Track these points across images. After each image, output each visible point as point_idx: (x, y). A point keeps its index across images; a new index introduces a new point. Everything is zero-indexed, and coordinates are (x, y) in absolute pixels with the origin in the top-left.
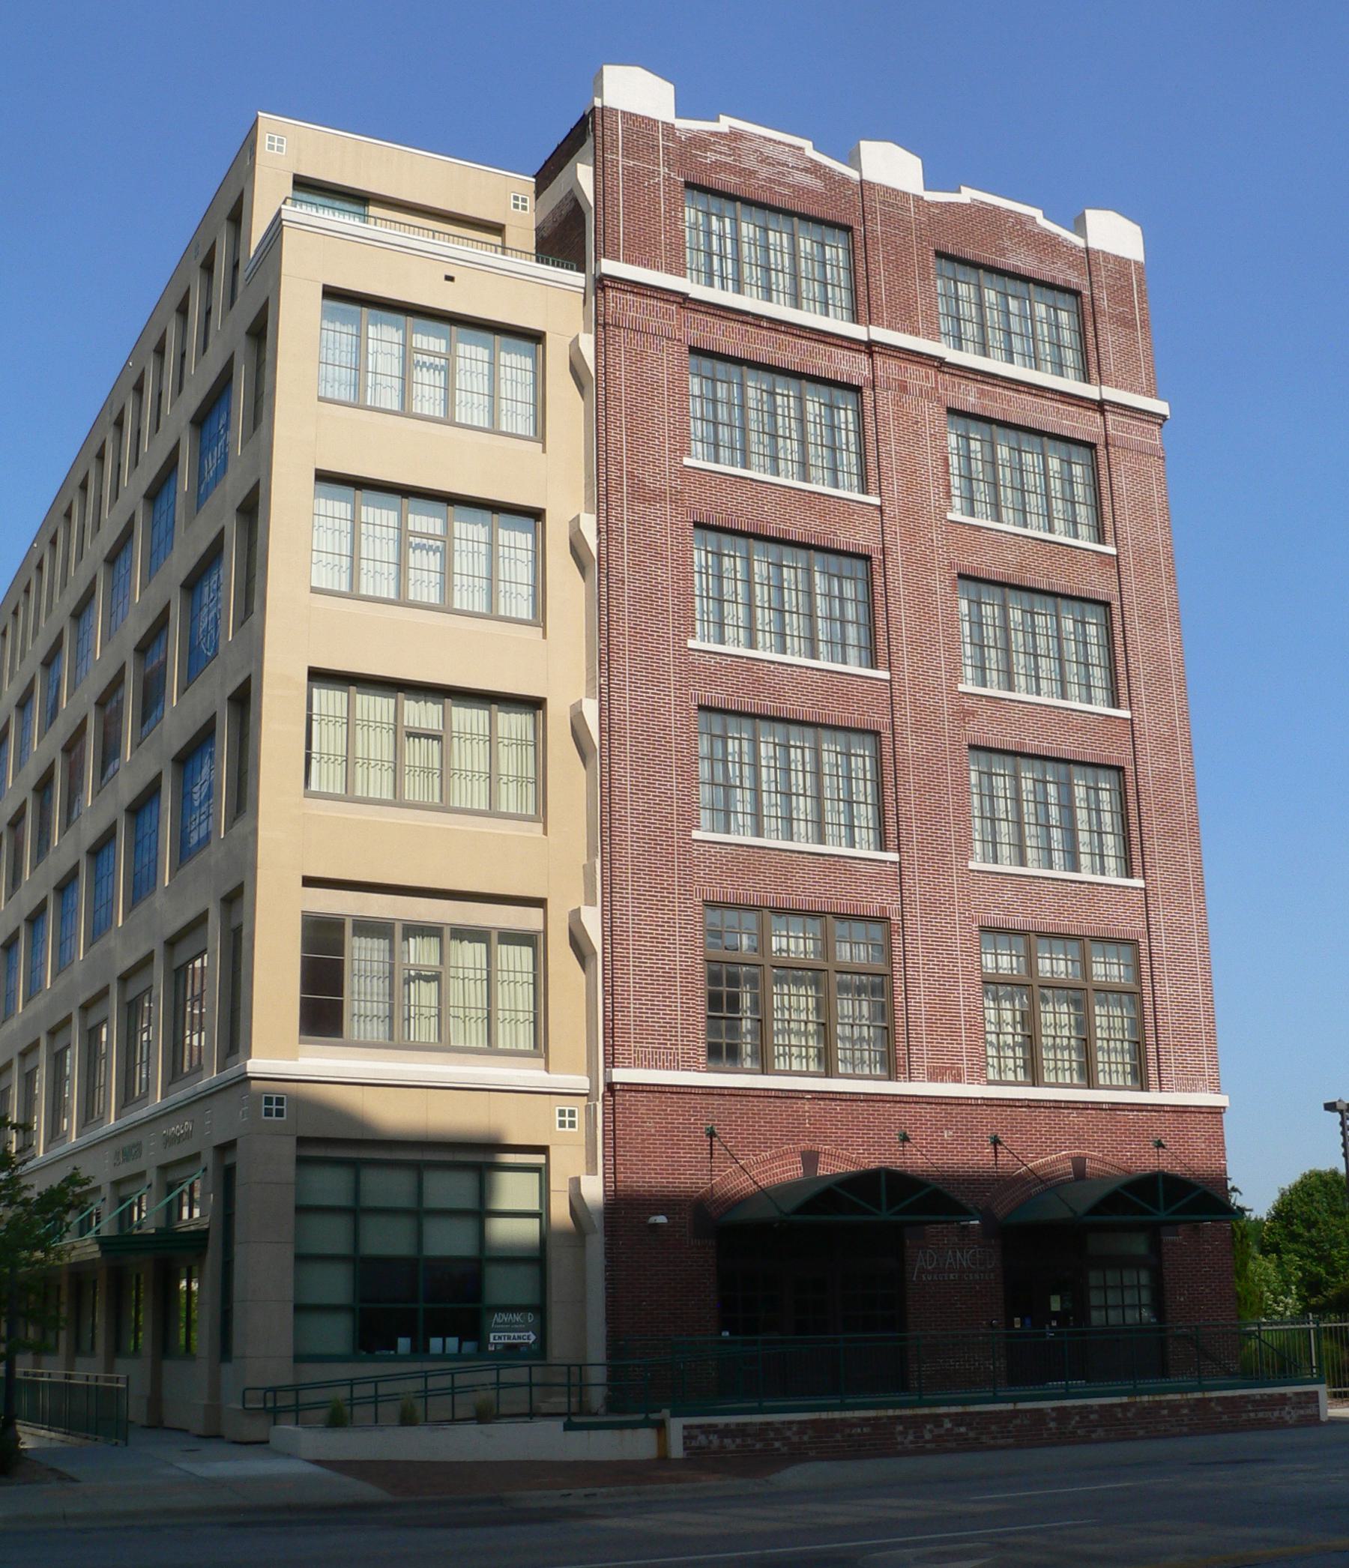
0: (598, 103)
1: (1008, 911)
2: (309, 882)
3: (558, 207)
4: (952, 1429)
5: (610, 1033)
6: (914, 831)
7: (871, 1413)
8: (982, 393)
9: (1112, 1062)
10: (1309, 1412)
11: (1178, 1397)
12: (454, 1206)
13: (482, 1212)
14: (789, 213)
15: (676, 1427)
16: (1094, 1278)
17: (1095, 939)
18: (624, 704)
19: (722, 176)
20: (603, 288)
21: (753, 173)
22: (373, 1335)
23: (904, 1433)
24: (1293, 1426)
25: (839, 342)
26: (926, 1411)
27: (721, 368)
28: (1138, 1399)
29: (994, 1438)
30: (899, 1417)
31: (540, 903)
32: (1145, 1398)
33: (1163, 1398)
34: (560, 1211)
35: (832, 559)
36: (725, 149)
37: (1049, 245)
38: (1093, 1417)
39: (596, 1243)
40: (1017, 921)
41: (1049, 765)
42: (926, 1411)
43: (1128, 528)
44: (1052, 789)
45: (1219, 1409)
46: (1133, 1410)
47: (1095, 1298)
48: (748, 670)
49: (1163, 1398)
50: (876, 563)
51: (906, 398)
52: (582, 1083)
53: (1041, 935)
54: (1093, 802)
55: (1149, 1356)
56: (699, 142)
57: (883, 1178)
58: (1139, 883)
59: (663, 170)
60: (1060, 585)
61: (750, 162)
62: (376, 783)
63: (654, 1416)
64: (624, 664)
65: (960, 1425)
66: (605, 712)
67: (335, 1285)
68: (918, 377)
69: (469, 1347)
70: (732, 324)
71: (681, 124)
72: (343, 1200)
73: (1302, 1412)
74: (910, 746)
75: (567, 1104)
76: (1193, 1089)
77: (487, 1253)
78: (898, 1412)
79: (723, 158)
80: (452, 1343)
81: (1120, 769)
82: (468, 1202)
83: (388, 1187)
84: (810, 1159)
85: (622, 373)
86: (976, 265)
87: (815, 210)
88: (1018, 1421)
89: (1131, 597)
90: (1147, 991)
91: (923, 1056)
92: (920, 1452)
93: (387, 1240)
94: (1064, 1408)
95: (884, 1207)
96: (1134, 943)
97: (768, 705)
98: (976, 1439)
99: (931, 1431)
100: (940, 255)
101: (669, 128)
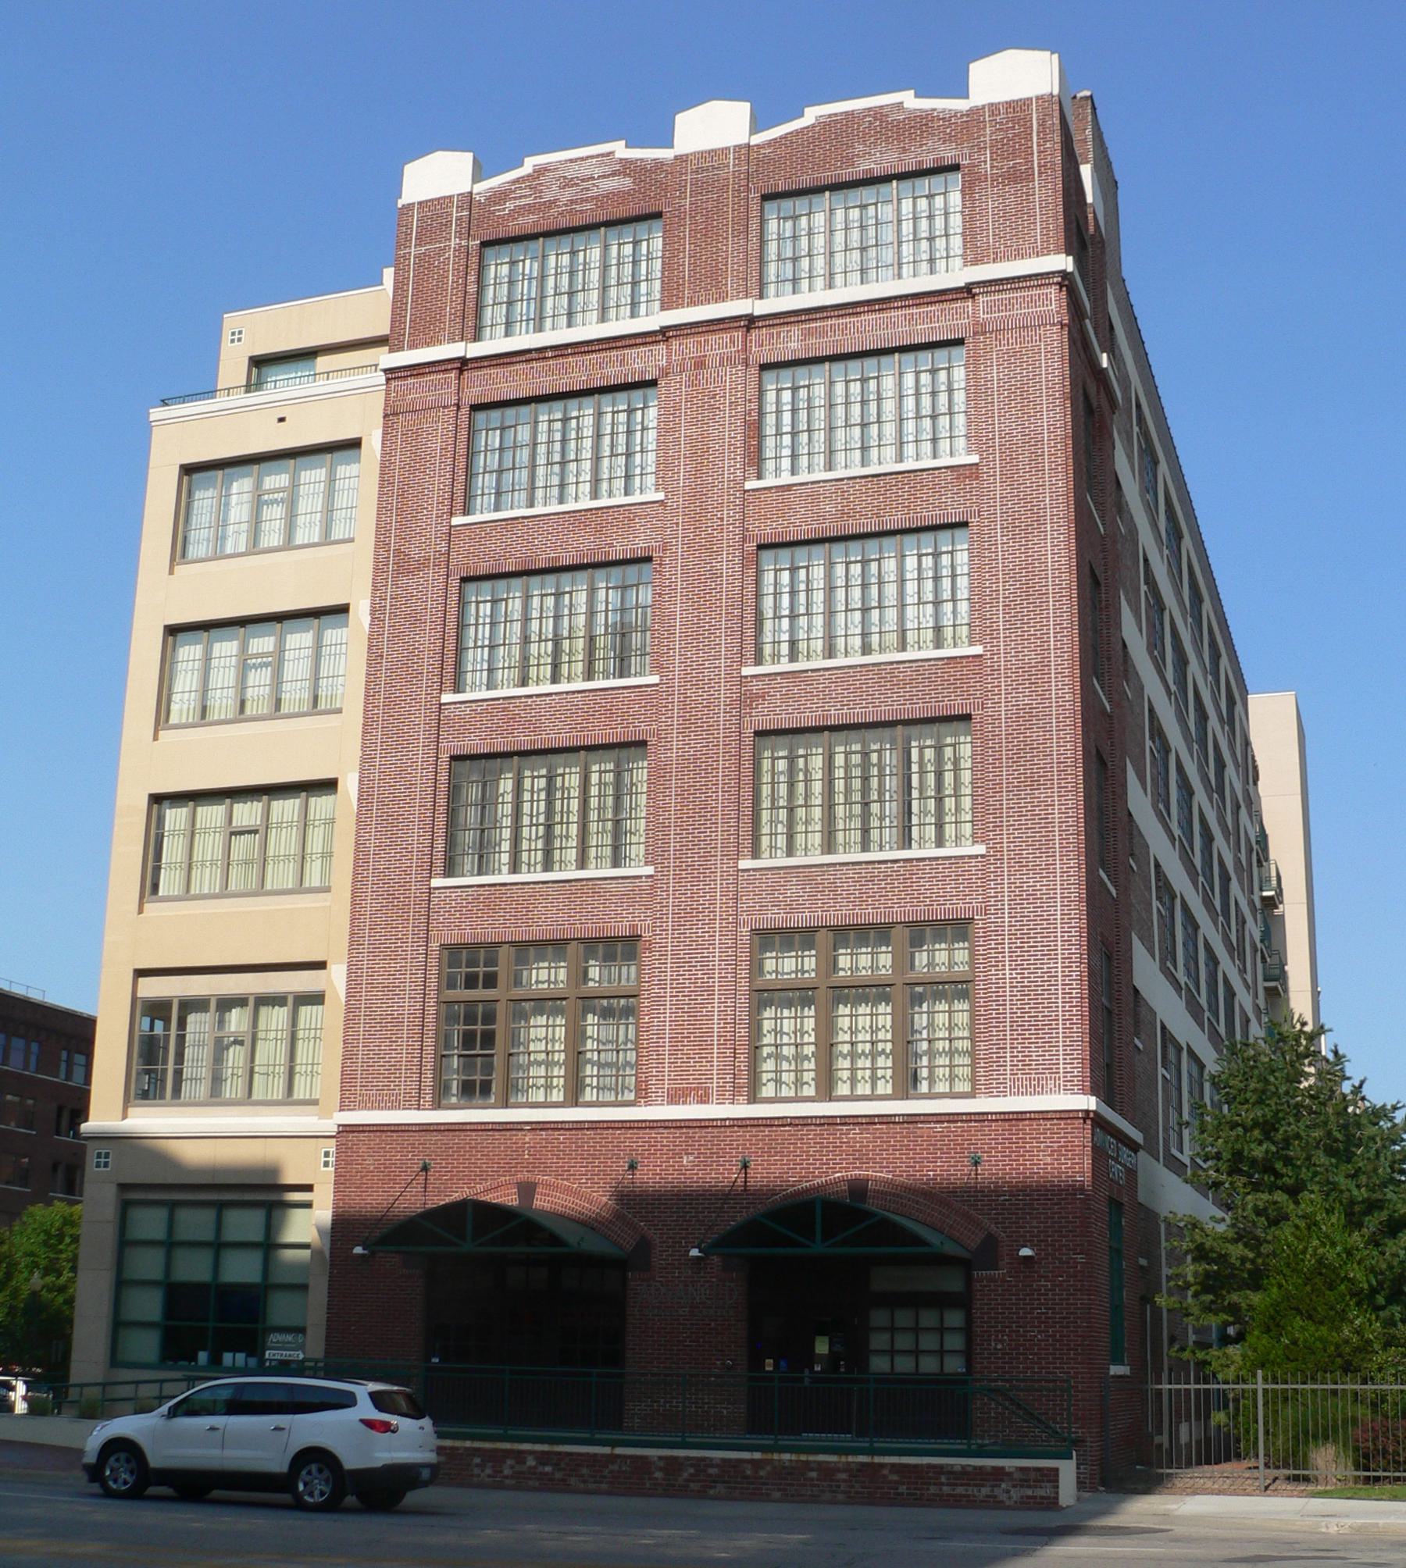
4: (535, 1467)
10: (1040, 1492)
11: (833, 1458)
19: (521, 220)
21: (552, 203)
22: (177, 1347)
23: (482, 1466)
24: (1009, 1508)
25: (633, 342)
26: (507, 1446)
28: (776, 1456)
29: (585, 1482)
30: (478, 1449)
32: (786, 1456)
33: (811, 1458)
35: (616, 572)
36: (527, 192)
38: (712, 1471)
42: (507, 1446)
45: (895, 1477)
46: (769, 1468)
47: (879, 1341)
48: (504, 709)
49: (811, 1458)
55: (935, 1410)
57: (470, 1210)
62: (206, 880)
65: (544, 1464)
67: (148, 1305)
70: (518, 367)
72: (208, 1235)
73: (1029, 1492)
76: (1038, 1089)
77: (277, 1278)
78: (477, 1444)
79: (523, 202)
80: (240, 1357)
82: (257, 1236)
83: (195, 1224)
88: (616, 1467)
92: (500, 1486)
93: (193, 1268)
94: (675, 1458)
95: (818, 1236)
97: (523, 740)
98: (564, 1480)
99: (512, 1467)
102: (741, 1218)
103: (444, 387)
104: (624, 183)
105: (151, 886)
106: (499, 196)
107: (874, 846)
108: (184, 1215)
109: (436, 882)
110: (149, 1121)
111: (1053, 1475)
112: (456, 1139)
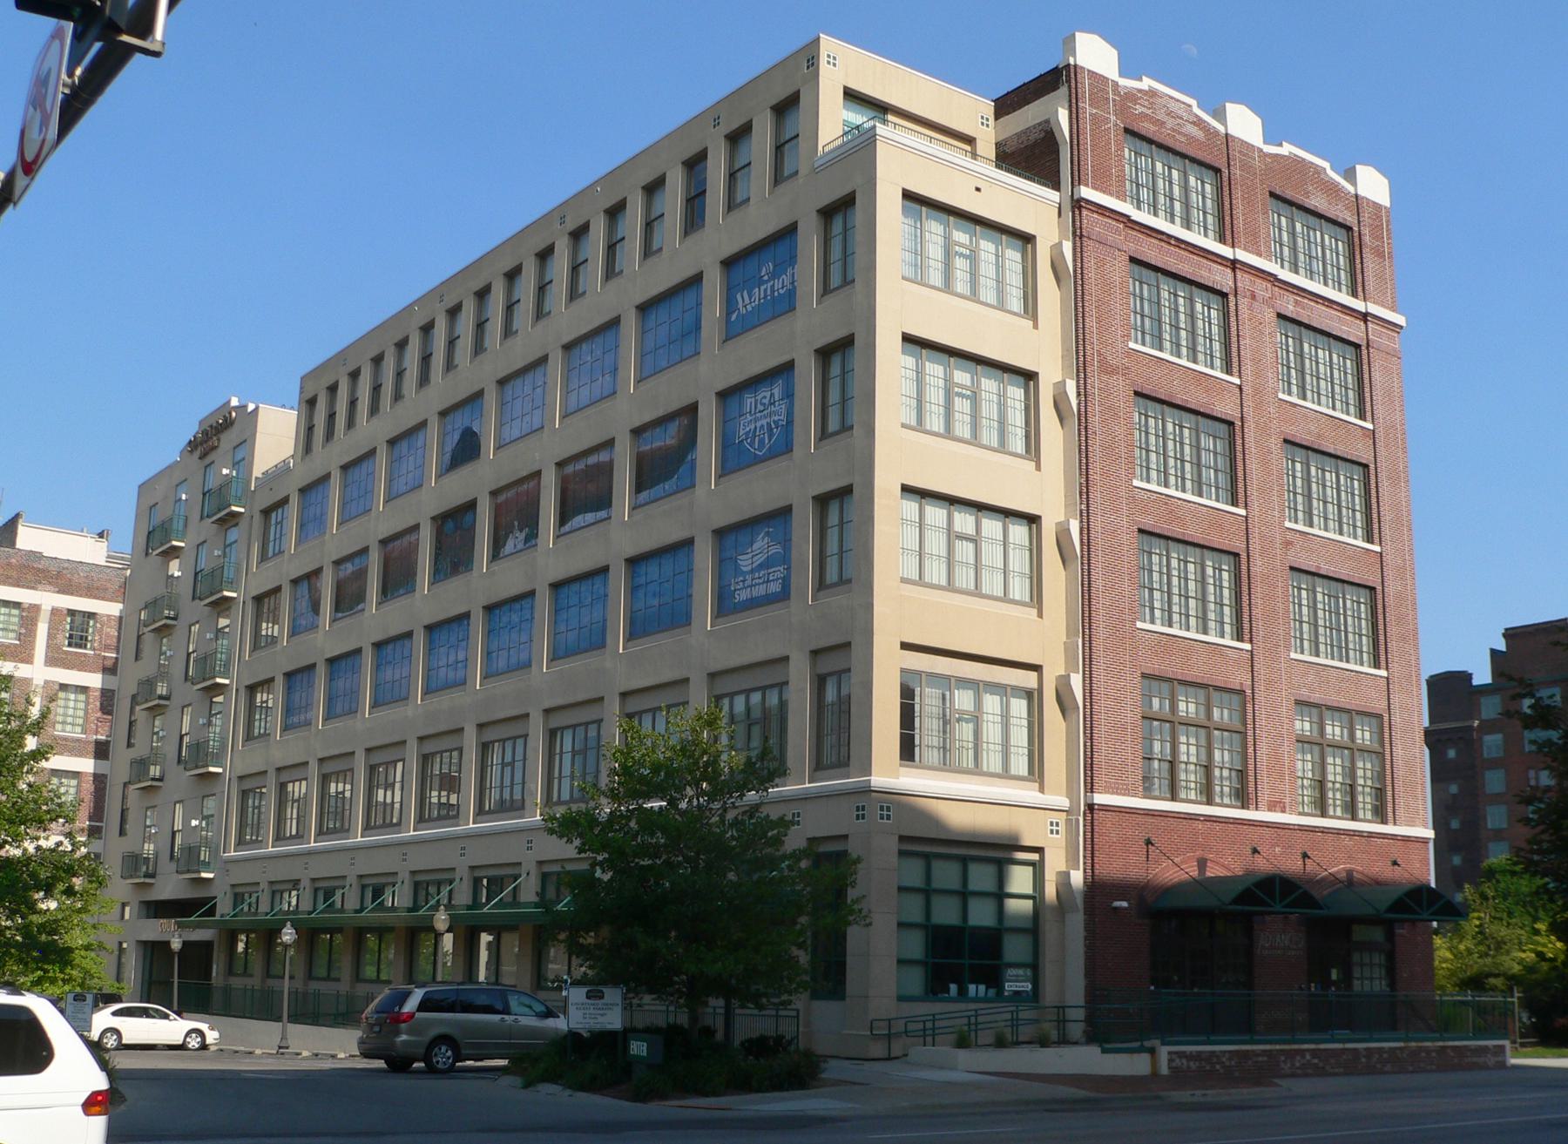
0: (1072, 61)
1: (1312, 691)
2: (905, 646)
3: (1024, 132)
5: (1090, 767)
6: (1259, 626)
7: (1268, 1047)
8: (1296, 302)
13: (1000, 895)
14: (1183, 156)
15: (1164, 1052)
16: (1356, 957)
17: (1359, 713)
18: (1097, 524)
19: (1145, 124)
20: (1080, 208)
27: (1145, 272)
31: (1036, 668)
32: (1413, 1044)
34: (1050, 891)
37: (1333, 190)
39: (1077, 922)
40: (1316, 697)
41: (1304, 577)
43: (1380, 410)
44: (1191, 567)
50: (1238, 428)
51: (1256, 304)
52: (1064, 802)
53: (1329, 708)
54: (1355, 607)
56: (1131, 96)
58: (1383, 673)
59: (1113, 118)
61: (1161, 116)
63: (1147, 1044)
64: (1096, 495)
66: (1086, 530)
68: (1261, 288)
69: (992, 992)
71: (1123, 82)
74: (1258, 566)
75: (1056, 817)
77: (1007, 924)
81: (1372, 589)
84: (1202, 864)
85: (1091, 274)
86: (1291, 203)
87: (1200, 155)
89: (1382, 464)
90: (1388, 751)
91: (1265, 795)
93: (946, 913)
96: (1380, 717)
97: (1176, 530)
100: (1272, 194)
101: (1116, 84)
102: (1241, 888)
104: (1199, 134)
107: (1176, 625)
108: (938, 867)
110: (909, 780)
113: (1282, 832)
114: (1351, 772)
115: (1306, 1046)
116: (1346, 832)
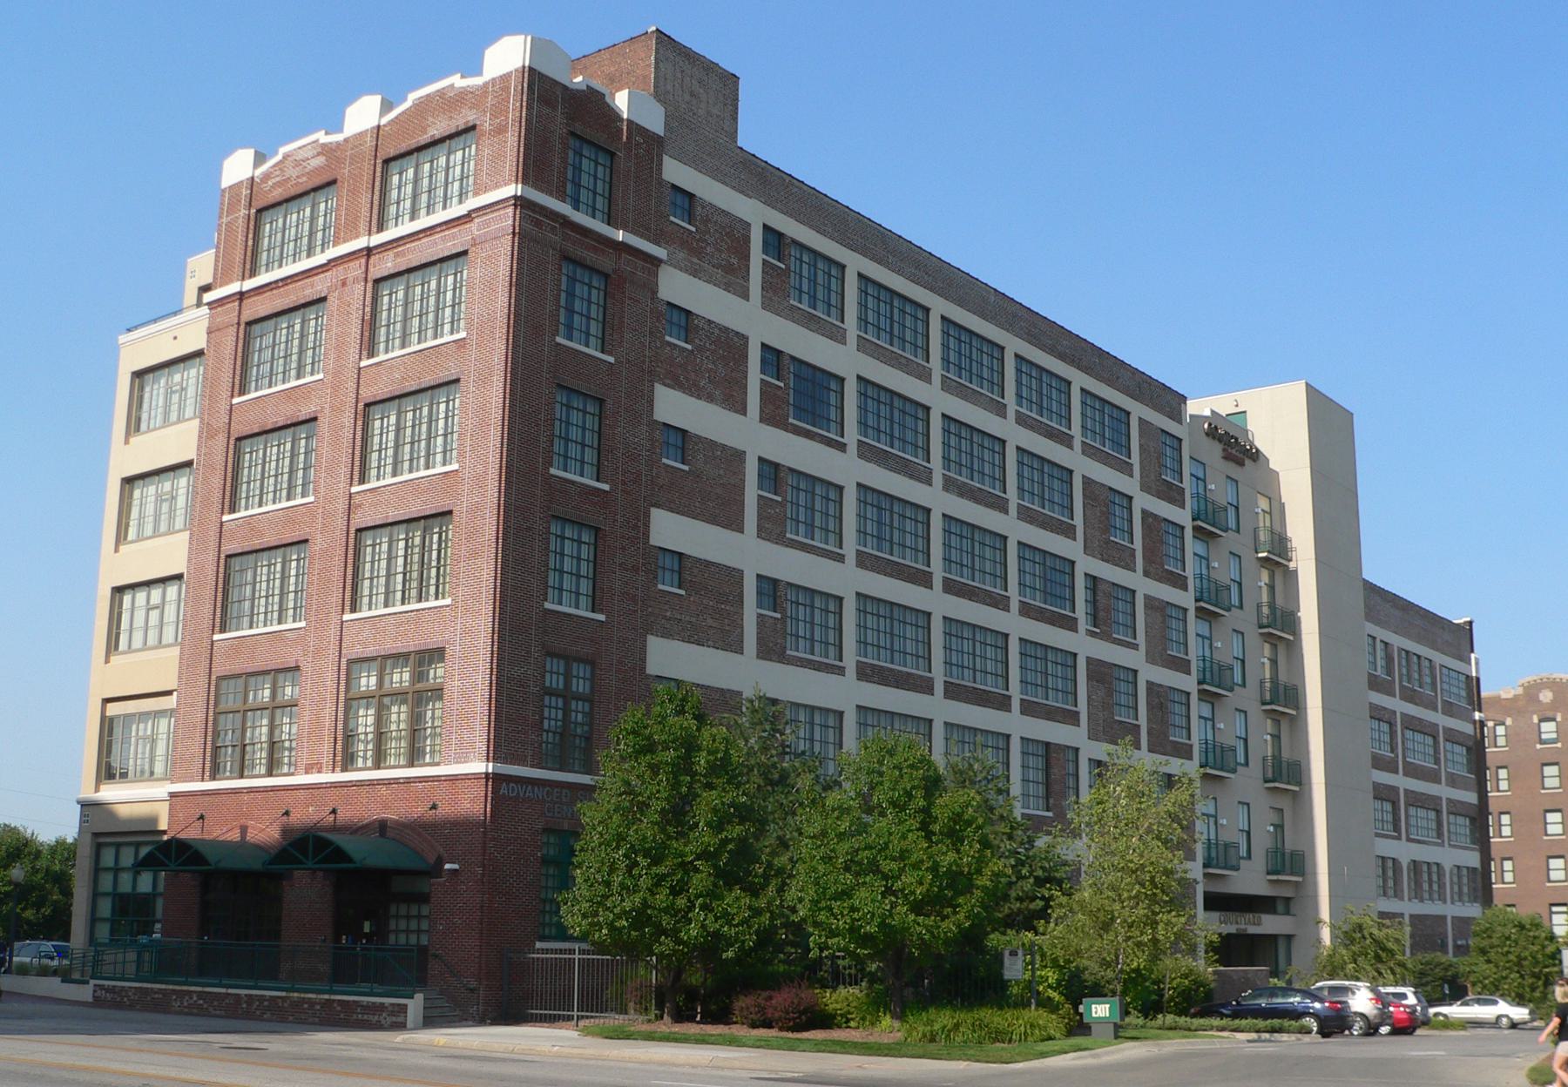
9: (397, 747)
12: (833, 371)
60: (428, 380)
84: (244, 830)
103: (355, 269)
104: (320, 161)
105: (112, 645)
106: (266, 176)
109: (216, 637)
111: (404, 1008)
112: (216, 799)
113: (316, 792)
114: (380, 721)
115: (193, 988)
116: (380, 782)
